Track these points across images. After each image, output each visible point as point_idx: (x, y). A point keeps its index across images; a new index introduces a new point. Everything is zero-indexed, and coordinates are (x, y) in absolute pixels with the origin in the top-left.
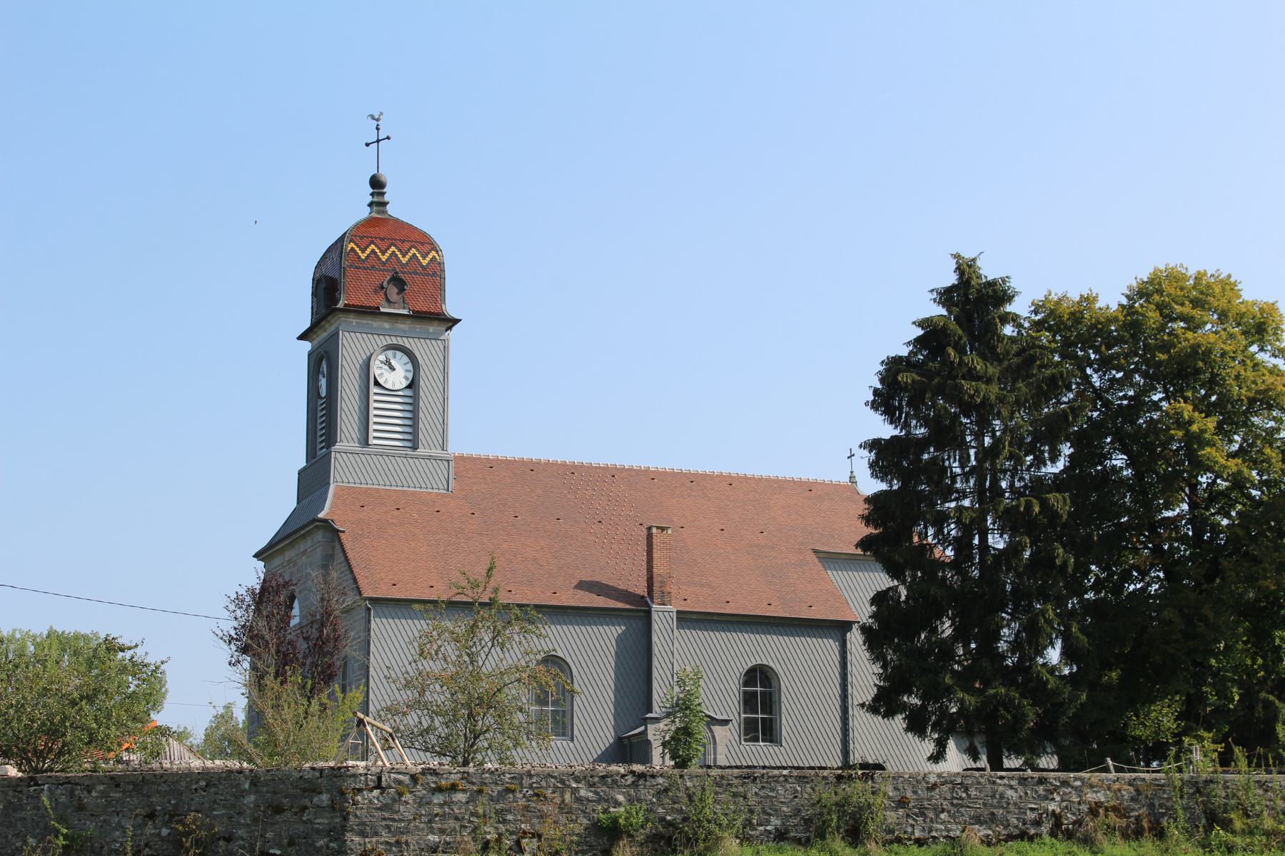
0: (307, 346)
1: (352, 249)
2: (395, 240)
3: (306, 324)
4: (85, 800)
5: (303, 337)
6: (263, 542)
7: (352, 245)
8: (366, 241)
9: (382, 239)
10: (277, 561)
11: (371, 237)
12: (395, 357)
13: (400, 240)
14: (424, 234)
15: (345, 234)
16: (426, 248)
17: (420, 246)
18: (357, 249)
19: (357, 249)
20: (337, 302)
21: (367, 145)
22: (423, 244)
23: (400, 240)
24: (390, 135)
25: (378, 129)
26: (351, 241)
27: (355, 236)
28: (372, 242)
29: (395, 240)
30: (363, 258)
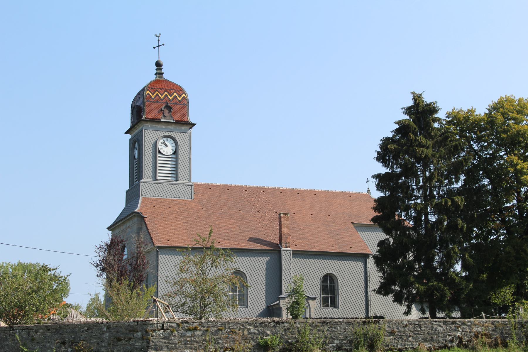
0: (129, 136)
1: (148, 94)
2: (167, 89)
5: (127, 132)
7: (148, 92)
9: (161, 89)
10: (117, 231)
11: (165, 89)
12: (167, 141)
13: (169, 89)
16: (180, 93)
18: (150, 94)
20: (142, 117)
21: (154, 48)
23: (169, 89)
26: (148, 90)
27: (149, 88)
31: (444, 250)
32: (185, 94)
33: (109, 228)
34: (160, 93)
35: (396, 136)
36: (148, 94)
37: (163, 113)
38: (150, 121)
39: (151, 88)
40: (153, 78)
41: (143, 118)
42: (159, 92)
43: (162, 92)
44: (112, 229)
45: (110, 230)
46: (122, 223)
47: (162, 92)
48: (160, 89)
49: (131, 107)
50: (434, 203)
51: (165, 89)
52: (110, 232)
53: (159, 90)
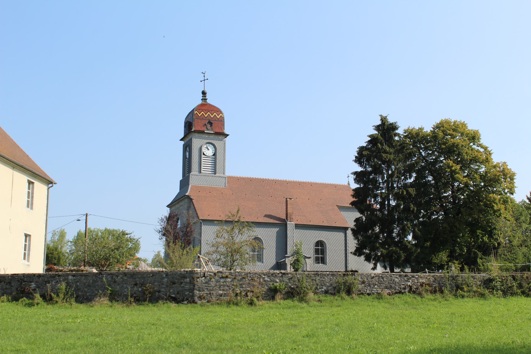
0: (183, 142)
1: (196, 113)
3: (182, 136)
6: (169, 202)
7: (196, 112)
9: (205, 110)
10: (173, 208)
14: (218, 109)
15: (194, 109)
16: (219, 113)
18: (198, 113)
19: (198, 113)
20: (192, 129)
21: (201, 81)
25: (204, 76)
26: (196, 111)
32: (222, 114)
33: (168, 206)
37: (206, 127)
43: (206, 112)
46: (177, 203)
47: (206, 112)
53: (204, 111)
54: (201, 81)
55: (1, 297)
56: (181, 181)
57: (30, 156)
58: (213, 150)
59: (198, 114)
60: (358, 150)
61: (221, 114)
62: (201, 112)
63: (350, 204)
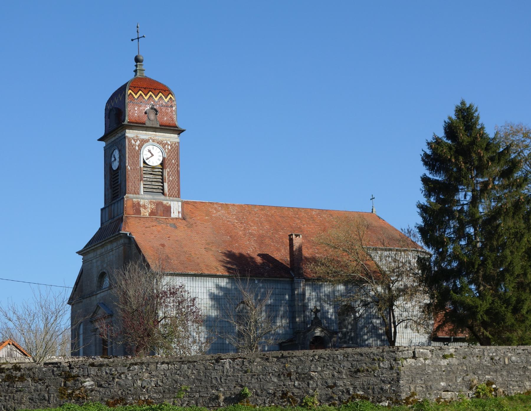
0: (103, 144)
1: (131, 93)
2: (151, 89)
3: (102, 133)
4: (311, 340)
5: (101, 139)
6: (81, 247)
7: (130, 91)
8: (137, 89)
9: (145, 88)
10: (91, 255)
11: (139, 87)
12: (153, 149)
13: (153, 89)
14: (165, 86)
15: (127, 83)
16: (167, 92)
17: (164, 93)
18: (133, 93)
19: (133, 93)
20: (124, 121)
21: (132, 40)
22: (165, 91)
23: (153, 89)
24: (145, 36)
25: (138, 32)
26: (130, 89)
27: (131, 86)
28: (140, 90)
29: (151, 89)
30: (150, 92)
31: (463, 174)
32: (172, 95)
33: (79, 253)
34: (143, 93)
35: (497, 204)
36: (131, 93)
37: (148, 116)
38: (170, 126)
39: (133, 87)
40: (131, 76)
41: (126, 123)
42: (142, 92)
43: (146, 92)
44: (84, 253)
45: (81, 255)
46: (101, 246)
47: (146, 92)
48: (143, 88)
49: (106, 109)
50: (445, 140)
51: (149, 88)
52: (82, 257)
53: (143, 89)
54: (132, 40)
55: (530, 211)
56: (102, 210)
57: (111, 95)
58: (159, 156)
59: (133, 96)
60: (476, 114)
61: (170, 96)
62: (138, 92)
63: (259, 255)
